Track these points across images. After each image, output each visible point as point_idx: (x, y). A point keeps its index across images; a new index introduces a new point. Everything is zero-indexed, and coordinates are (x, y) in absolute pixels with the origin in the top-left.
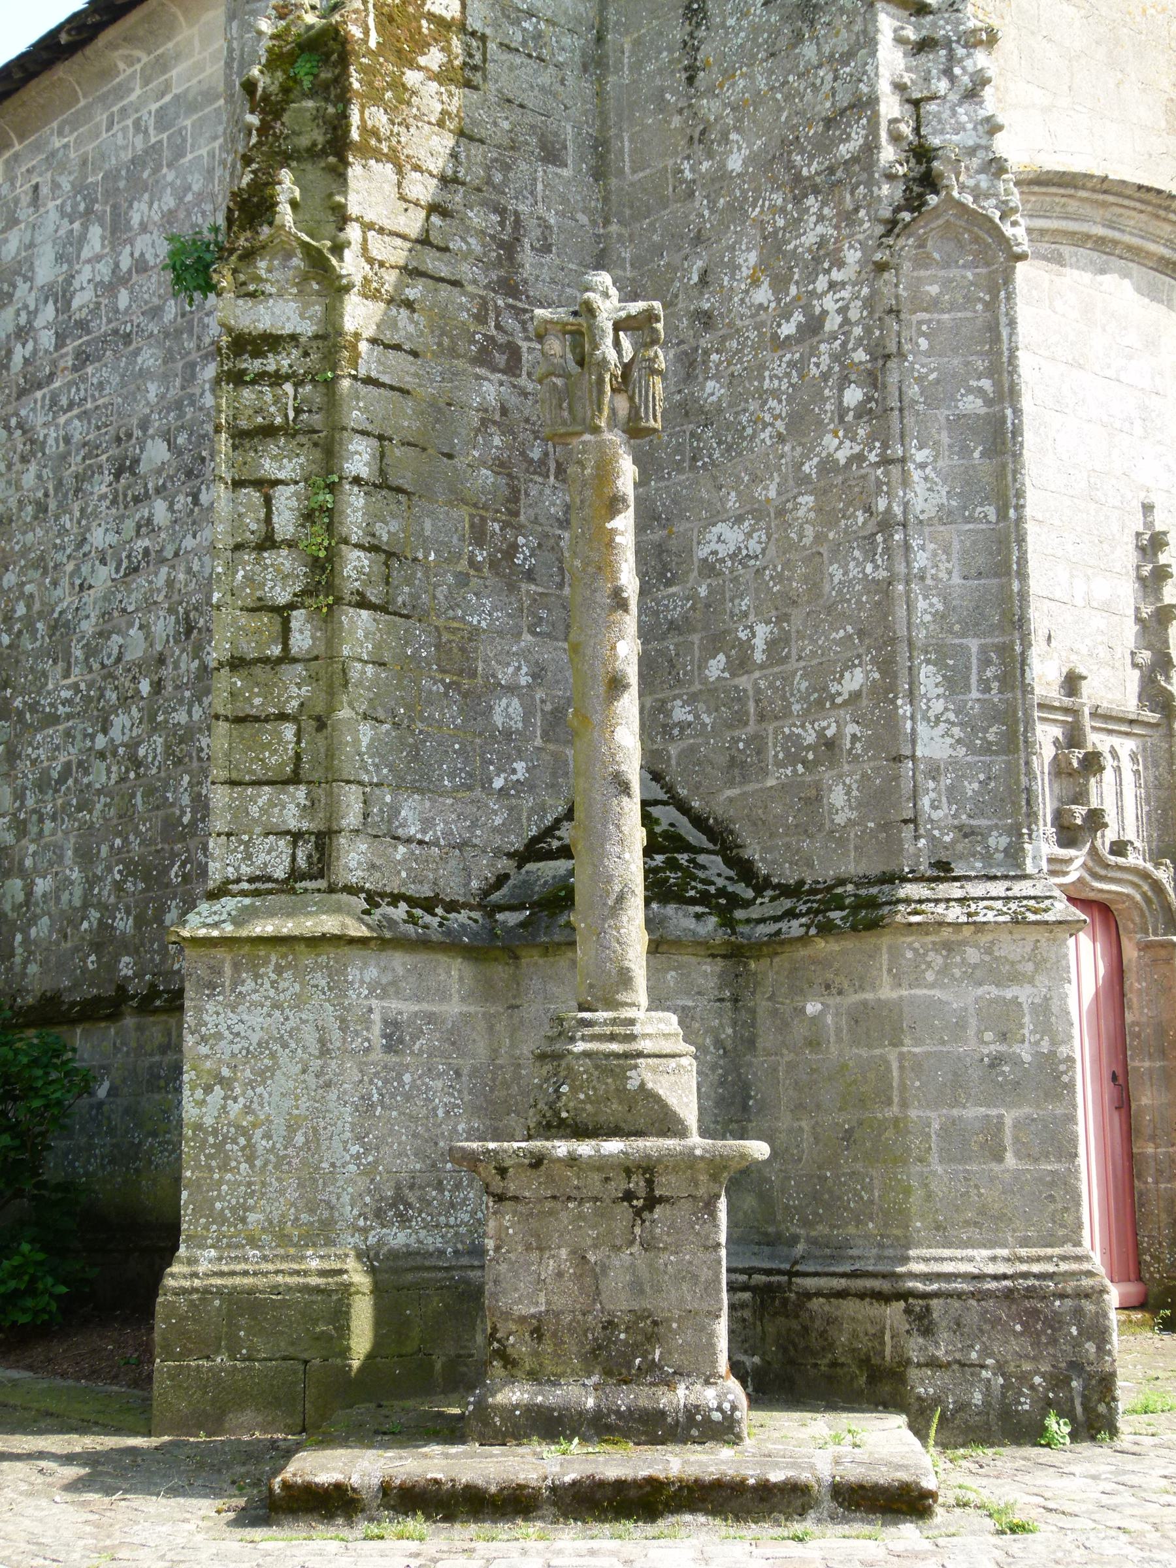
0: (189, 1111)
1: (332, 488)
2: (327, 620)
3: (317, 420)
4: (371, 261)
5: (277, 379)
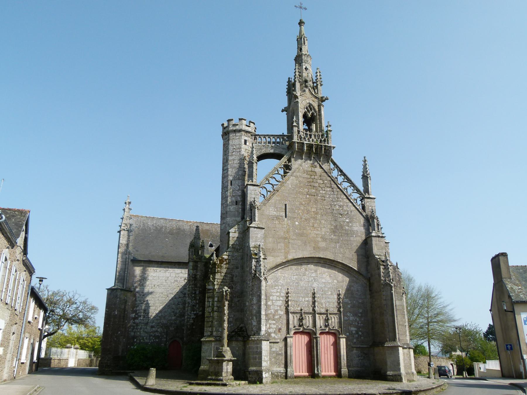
0: (202, 355)
1: (214, 302)
2: (213, 313)
3: (213, 296)
4: (218, 282)
5: (210, 293)
